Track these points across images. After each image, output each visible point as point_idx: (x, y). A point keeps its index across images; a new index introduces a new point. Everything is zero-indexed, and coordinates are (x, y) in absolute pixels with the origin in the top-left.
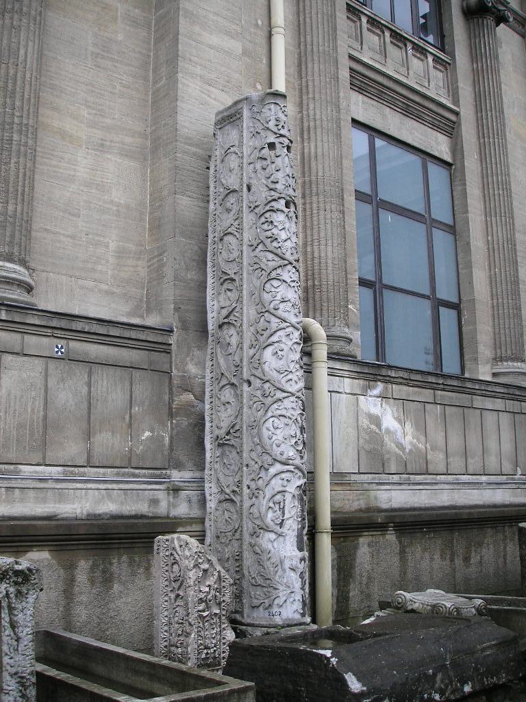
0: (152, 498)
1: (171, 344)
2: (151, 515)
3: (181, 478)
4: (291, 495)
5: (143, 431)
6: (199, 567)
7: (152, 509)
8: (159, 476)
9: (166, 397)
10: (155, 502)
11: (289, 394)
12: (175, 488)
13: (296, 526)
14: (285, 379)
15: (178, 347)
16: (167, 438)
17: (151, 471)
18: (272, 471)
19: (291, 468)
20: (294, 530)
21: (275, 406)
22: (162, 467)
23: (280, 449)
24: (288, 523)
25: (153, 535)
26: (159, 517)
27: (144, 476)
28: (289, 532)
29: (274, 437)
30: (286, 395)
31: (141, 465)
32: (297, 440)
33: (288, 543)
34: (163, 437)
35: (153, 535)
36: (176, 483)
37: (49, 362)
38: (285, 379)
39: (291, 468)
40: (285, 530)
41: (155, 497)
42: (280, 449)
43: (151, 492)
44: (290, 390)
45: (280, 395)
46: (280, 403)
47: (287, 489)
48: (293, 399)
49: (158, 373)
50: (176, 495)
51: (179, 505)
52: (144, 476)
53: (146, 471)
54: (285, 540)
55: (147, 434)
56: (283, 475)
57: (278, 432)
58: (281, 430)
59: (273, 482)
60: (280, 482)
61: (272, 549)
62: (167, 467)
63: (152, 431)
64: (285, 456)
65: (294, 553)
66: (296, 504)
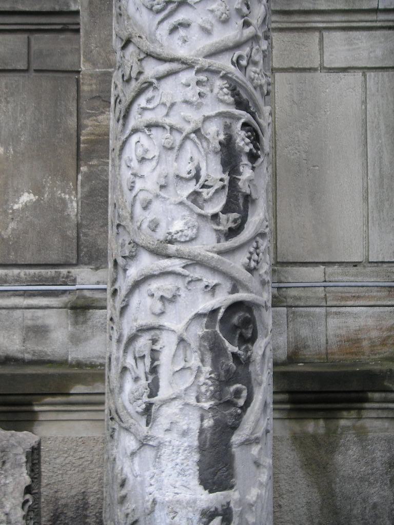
0: (30, 323)
1: (77, 13)
2: (27, 356)
3: (98, 283)
4: (174, 339)
5: (18, 193)
6: (264, 466)
7: (31, 346)
8: (53, 281)
9: (72, 122)
10: (39, 331)
11: (175, 66)
12: (81, 302)
13: (192, 422)
14: (167, 25)
15: (92, 15)
16: (75, 204)
17: (32, 271)
18: (134, 272)
19: (176, 265)
20: (184, 434)
21: (142, 102)
22: (62, 260)
23: (149, 216)
24: (167, 414)
25: (28, 398)
26: (51, 363)
27: (18, 280)
28: (168, 437)
29: (139, 185)
30: (164, 68)
31: (12, 258)
32: (197, 188)
33: (167, 465)
34: (63, 201)
35: (28, 398)
36: (88, 294)
37: (368, 74)
38: (167, 25)
39: (176, 265)
40: (158, 431)
41: (39, 322)
42: (149, 216)
43: (29, 313)
44: (182, 52)
45: (152, 69)
46: (149, 94)
47: (165, 321)
48: (188, 76)
49: (50, 75)
50: (81, 319)
51: (87, 339)
52: (18, 280)
53: (22, 273)
54: (158, 457)
55: (27, 198)
56: (154, 285)
57: (146, 169)
58: (154, 163)
59: (135, 300)
60: (149, 301)
61: (130, 476)
62: (74, 262)
63: (37, 190)
64: (161, 234)
65: (186, 496)
66: (195, 361)
